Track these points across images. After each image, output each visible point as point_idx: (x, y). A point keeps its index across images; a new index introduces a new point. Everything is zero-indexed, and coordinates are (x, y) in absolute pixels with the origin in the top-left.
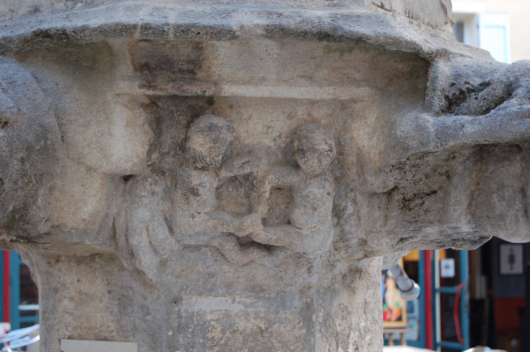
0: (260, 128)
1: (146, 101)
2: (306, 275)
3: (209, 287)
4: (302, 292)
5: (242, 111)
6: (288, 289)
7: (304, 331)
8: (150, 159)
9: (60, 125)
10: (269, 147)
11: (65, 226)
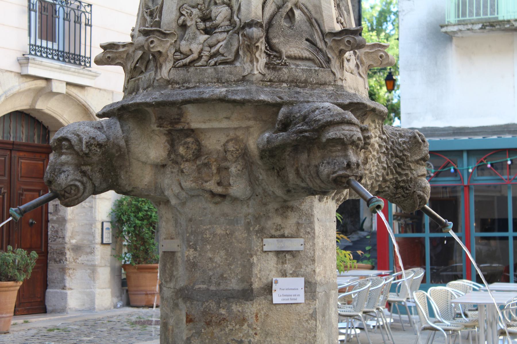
0: (215, 142)
1: (166, 132)
2: (246, 209)
3: (204, 214)
4: (245, 217)
5: (206, 134)
6: (239, 215)
7: (246, 235)
8: (171, 157)
9: (127, 145)
10: (220, 150)
11: (139, 187)
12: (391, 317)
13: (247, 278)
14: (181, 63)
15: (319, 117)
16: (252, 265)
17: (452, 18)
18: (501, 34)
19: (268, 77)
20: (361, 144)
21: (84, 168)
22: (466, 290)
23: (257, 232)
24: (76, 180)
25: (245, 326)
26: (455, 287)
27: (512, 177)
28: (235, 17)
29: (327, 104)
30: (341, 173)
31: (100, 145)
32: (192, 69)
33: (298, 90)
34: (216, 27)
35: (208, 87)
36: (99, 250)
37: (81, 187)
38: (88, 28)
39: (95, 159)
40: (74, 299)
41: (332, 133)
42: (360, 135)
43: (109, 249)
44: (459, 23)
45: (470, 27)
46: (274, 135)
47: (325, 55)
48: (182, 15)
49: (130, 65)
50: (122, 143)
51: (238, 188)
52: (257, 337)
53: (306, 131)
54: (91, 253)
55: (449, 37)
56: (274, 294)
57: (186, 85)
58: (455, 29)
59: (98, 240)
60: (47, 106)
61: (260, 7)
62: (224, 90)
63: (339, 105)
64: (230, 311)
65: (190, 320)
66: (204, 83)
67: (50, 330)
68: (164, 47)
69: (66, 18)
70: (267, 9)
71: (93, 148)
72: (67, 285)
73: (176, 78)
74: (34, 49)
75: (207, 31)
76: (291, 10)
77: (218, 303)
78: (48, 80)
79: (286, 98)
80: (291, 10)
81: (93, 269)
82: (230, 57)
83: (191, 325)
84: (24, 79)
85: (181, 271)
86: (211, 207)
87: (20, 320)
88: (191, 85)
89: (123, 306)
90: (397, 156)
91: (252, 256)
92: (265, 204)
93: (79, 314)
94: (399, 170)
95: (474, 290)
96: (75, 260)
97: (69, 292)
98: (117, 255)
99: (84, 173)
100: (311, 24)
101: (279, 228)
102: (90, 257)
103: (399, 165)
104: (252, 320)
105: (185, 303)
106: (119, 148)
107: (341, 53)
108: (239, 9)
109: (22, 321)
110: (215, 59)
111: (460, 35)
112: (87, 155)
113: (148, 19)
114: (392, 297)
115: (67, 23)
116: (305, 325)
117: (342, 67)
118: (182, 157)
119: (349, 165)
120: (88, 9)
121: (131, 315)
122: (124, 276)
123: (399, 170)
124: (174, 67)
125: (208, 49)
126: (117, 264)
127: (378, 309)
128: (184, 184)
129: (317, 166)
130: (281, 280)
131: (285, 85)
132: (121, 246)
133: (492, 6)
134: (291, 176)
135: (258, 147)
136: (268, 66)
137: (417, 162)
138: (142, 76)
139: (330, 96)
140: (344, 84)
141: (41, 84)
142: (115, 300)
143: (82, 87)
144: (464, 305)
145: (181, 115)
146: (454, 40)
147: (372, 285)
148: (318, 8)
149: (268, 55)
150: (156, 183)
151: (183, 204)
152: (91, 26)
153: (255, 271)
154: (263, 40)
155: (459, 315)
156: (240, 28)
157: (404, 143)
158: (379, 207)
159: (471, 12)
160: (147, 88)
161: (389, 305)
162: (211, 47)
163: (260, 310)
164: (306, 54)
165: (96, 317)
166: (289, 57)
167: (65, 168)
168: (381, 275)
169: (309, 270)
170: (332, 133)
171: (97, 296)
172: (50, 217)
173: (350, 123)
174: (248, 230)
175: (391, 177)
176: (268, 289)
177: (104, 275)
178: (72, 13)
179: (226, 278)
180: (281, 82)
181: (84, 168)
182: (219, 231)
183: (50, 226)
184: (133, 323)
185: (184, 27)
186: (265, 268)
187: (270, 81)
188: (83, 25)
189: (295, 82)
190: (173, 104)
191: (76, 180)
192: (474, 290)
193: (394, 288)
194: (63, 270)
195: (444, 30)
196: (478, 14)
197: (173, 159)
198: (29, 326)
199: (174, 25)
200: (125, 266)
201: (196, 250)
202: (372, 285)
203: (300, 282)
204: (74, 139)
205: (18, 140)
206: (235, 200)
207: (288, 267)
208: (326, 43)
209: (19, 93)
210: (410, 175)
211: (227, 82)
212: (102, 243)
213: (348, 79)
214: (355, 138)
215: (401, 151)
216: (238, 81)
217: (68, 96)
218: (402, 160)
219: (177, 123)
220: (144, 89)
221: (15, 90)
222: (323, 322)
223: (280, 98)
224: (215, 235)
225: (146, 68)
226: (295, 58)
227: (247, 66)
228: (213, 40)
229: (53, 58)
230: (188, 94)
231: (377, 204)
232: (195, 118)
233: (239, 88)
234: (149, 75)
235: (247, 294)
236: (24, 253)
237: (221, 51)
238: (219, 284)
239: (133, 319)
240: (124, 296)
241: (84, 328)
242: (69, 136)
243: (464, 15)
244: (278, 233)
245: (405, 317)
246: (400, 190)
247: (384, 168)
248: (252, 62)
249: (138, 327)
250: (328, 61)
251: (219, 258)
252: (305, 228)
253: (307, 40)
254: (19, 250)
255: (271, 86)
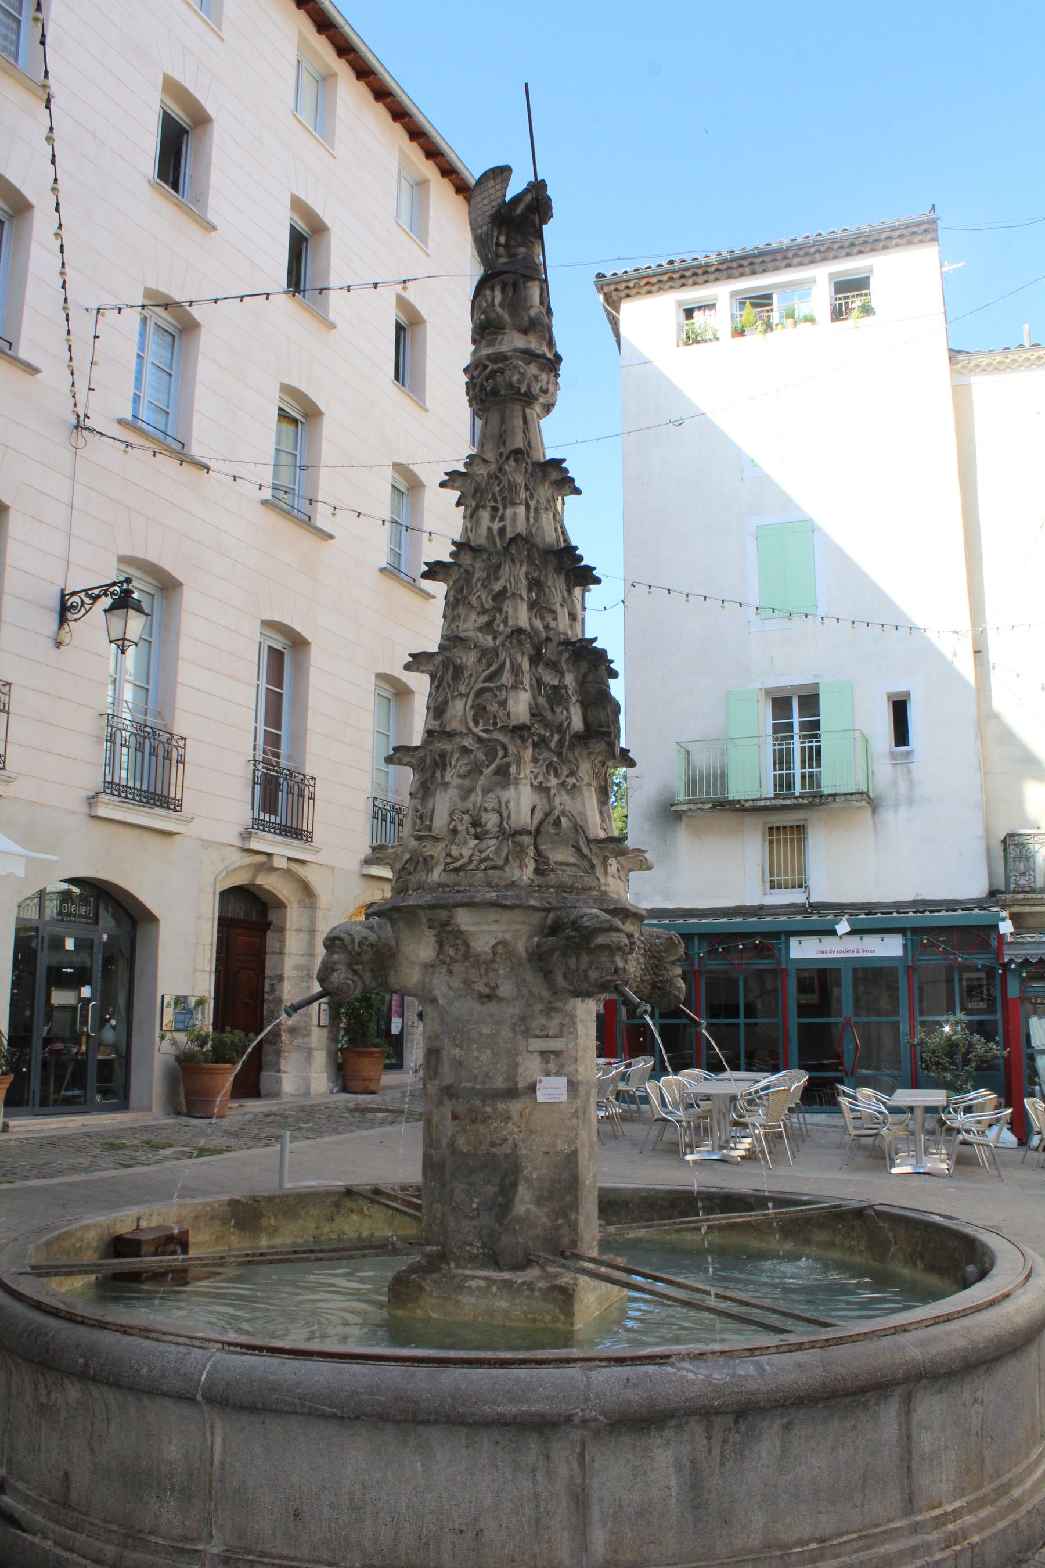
12: (619, 1107)
13: (512, 1077)
14: (451, 866)
15: (587, 924)
16: (517, 1064)
17: (682, 797)
18: (731, 814)
19: (537, 882)
20: (627, 949)
21: (356, 967)
22: (697, 1079)
23: (523, 1032)
24: (348, 979)
25: (510, 1124)
26: (686, 1076)
27: (743, 961)
28: (505, 824)
29: (594, 911)
30: (609, 978)
31: (371, 945)
32: (462, 873)
33: (565, 895)
34: (486, 833)
35: (478, 891)
36: (315, 1030)
37: (352, 985)
38: (311, 802)
39: (366, 958)
40: (289, 1084)
41: (600, 940)
42: (627, 941)
43: (326, 1030)
44: (689, 802)
45: (700, 806)
46: (543, 940)
47: (590, 861)
48: (453, 820)
49: (398, 866)
50: (393, 943)
51: (506, 989)
52: (522, 1135)
53: (575, 937)
54: (307, 1035)
55: (678, 816)
56: (538, 1093)
57: (457, 888)
58: (685, 807)
59: (315, 1022)
60: (267, 881)
61: (529, 814)
62: (494, 894)
63: (606, 911)
64: (494, 1109)
65: (455, 1117)
66: (475, 886)
67: (266, 1116)
68: (436, 850)
69: (290, 792)
70: (535, 816)
71: (365, 947)
72: (282, 1068)
73: (447, 881)
74: (258, 824)
75: (477, 837)
76: (558, 818)
77: (484, 1101)
78: (269, 855)
79: (554, 904)
80: (558, 818)
81: (309, 1052)
82: (500, 862)
83: (457, 1122)
84: (246, 854)
85: (446, 1069)
86: (478, 1006)
87: (235, 1104)
88: (461, 889)
89: (339, 1092)
90: (654, 957)
91: (517, 1056)
92: (531, 1005)
93: (293, 1099)
94: (656, 971)
95: (706, 1079)
96: (291, 1042)
97: (284, 1076)
98: (334, 1038)
99: (355, 972)
100: (577, 831)
101: (543, 1028)
102: (306, 1039)
103: (656, 966)
104: (516, 1118)
105: (451, 1100)
106: (390, 948)
107: (605, 860)
108: (509, 816)
109: (237, 1105)
110: (485, 864)
111: (690, 813)
112: (359, 954)
113: (418, 821)
114: (622, 1086)
115: (290, 796)
116: (567, 1122)
117: (606, 873)
118: (451, 958)
119: (616, 970)
120: (312, 782)
121: (348, 1101)
122: (340, 1060)
123: (656, 971)
124: (444, 870)
125: (478, 854)
126: (334, 1048)
127: (608, 1099)
128: (452, 984)
129: (585, 971)
130: (545, 1079)
131: (552, 890)
132: (338, 1029)
133: (723, 785)
134: (560, 979)
135: (527, 951)
136: (537, 871)
137: (673, 963)
138: (410, 877)
139: (595, 901)
140: (608, 889)
141: (262, 859)
142: (331, 1085)
143: (302, 862)
144: (696, 1095)
145: (451, 917)
146: (684, 819)
147: (603, 1075)
148: (583, 815)
149: (536, 861)
150: (424, 983)
151: (450, 1003)
152: (314, 800)
153: (521, 1070)
154: (532, 847)
155: (692, 1105)
156: (509, 834)
157: (661, 944)
158: (646, 1012)
159: (701, 791)
160: (418, 889)
161: (618, 1095)
162: (481, 852)
163: (524, 1109)
164: (572, 860)
165: (312, 1102)
166: (556, 863)
167: (338, 967)
168: (610, 1064)
169: (571, 1069)
170: (600, 940)
171: (313, 1080)
172: (266, 996)
173: (618, 930)
174: (513, 1030)
175: (648, 977)
176: (532, 1088)
177: (320, 1058)
178: (296, 786)
179: (491, 1077)
180: (548, 887)
181: (356, 967)
182: (486, 1030)
183: (266, 1007)
184: (351, 1111)
185: (455, 831)
186: (530, 1067)
187: (538, 886)
188: (306, 798)
189: (561, 888)
190: (444, 907)
191: (348, 979)
192: (706, 1079)
193: (624, 1077)
194: (278, 1053)
195: (673, 808)
196: (708, 793)
197: (442, 961)
198: (245, 1110)
199: (445, 829)
200: (341, 1050)
201: (462, 1048)
202: (603, 1075)
203: (563, 1081)
204: (347, 938)
205: (236, 916)
206: (501, 1000)
207: (552, 1066)
208: (590, 849)
209: (240, 868)
210: (667, 976)
211: (497, 886)
212: (319, 1025)
213: (611, 884)
214: (622, 944)
215: (659, 952)
216: (508, 885)
217: (288, 871)
218: (659, 961)
219: (447, 925)
220: (414, 891)
221: (236, 865)
222: (584, 1120)
223: (549, 903)
224: (481, 1034)
225: (415, 870)
226: (562, 864)
227: (517, 873)
228: (483, 846)
229: (275, 833)
230: (459, 897)
231: (644, 1008)
232: (463, 919)
233: (509, 893)
234: (420, 876)
235: (511, 1093)
236: (243, 1034)
237: (491, 856)
238: (484, 1083)
239: (352, 1105)
240: (340, 1081)
241: (301, 1114)
242: (342, 935)
243: (694, 793)
244: (542, 1033)
245: (634, 1107)
246: (657, 991)
247: (642, 969)
248: (521, 867)
249: (357, 1114)
250: (593, 866)
251: (486, 1056)
252: (568, 1028)
253: (573, 846)
254: (236, 1032)
255: (539, 891)
